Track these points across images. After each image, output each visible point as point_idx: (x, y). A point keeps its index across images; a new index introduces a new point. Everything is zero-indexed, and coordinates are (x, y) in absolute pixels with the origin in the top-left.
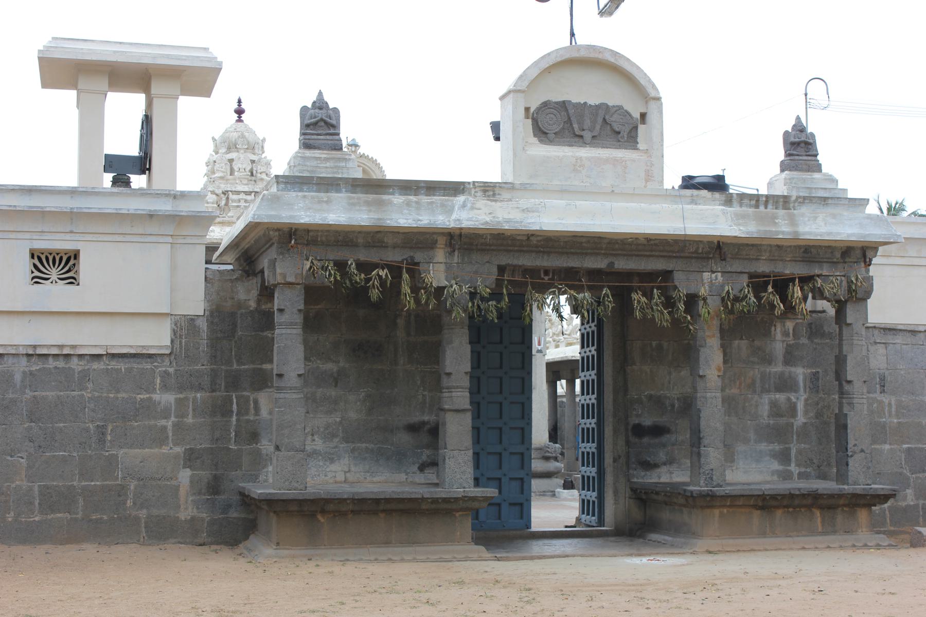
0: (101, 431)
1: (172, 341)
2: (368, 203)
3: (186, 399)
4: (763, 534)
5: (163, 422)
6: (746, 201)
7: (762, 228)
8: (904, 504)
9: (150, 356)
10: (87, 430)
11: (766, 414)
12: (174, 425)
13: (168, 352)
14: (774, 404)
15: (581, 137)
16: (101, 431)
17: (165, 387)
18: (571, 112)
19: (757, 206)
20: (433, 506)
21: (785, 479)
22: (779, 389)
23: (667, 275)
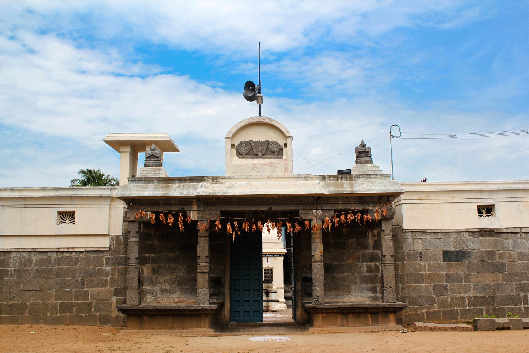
0: (83, 281)
1: (110, 246)
2: (162, 187)
3: (115, 268)
4: (343, 325)
5: (106, 278)
6: (332, 178)
7: (336, 189)
8: (433, 310)
9: (102, 251)
10: (77, 281)
11: (365, 271)
12: (111, 279)
13: (108, 250)
14: (369, 267)
15: (257, 155)
16: (83, 281)
17: (107, 264)
18: (252, 145)
19: (337, 180)
20: (190, 313)
21: (374, 300)
22: (371, 260)
23: (296, 213)
